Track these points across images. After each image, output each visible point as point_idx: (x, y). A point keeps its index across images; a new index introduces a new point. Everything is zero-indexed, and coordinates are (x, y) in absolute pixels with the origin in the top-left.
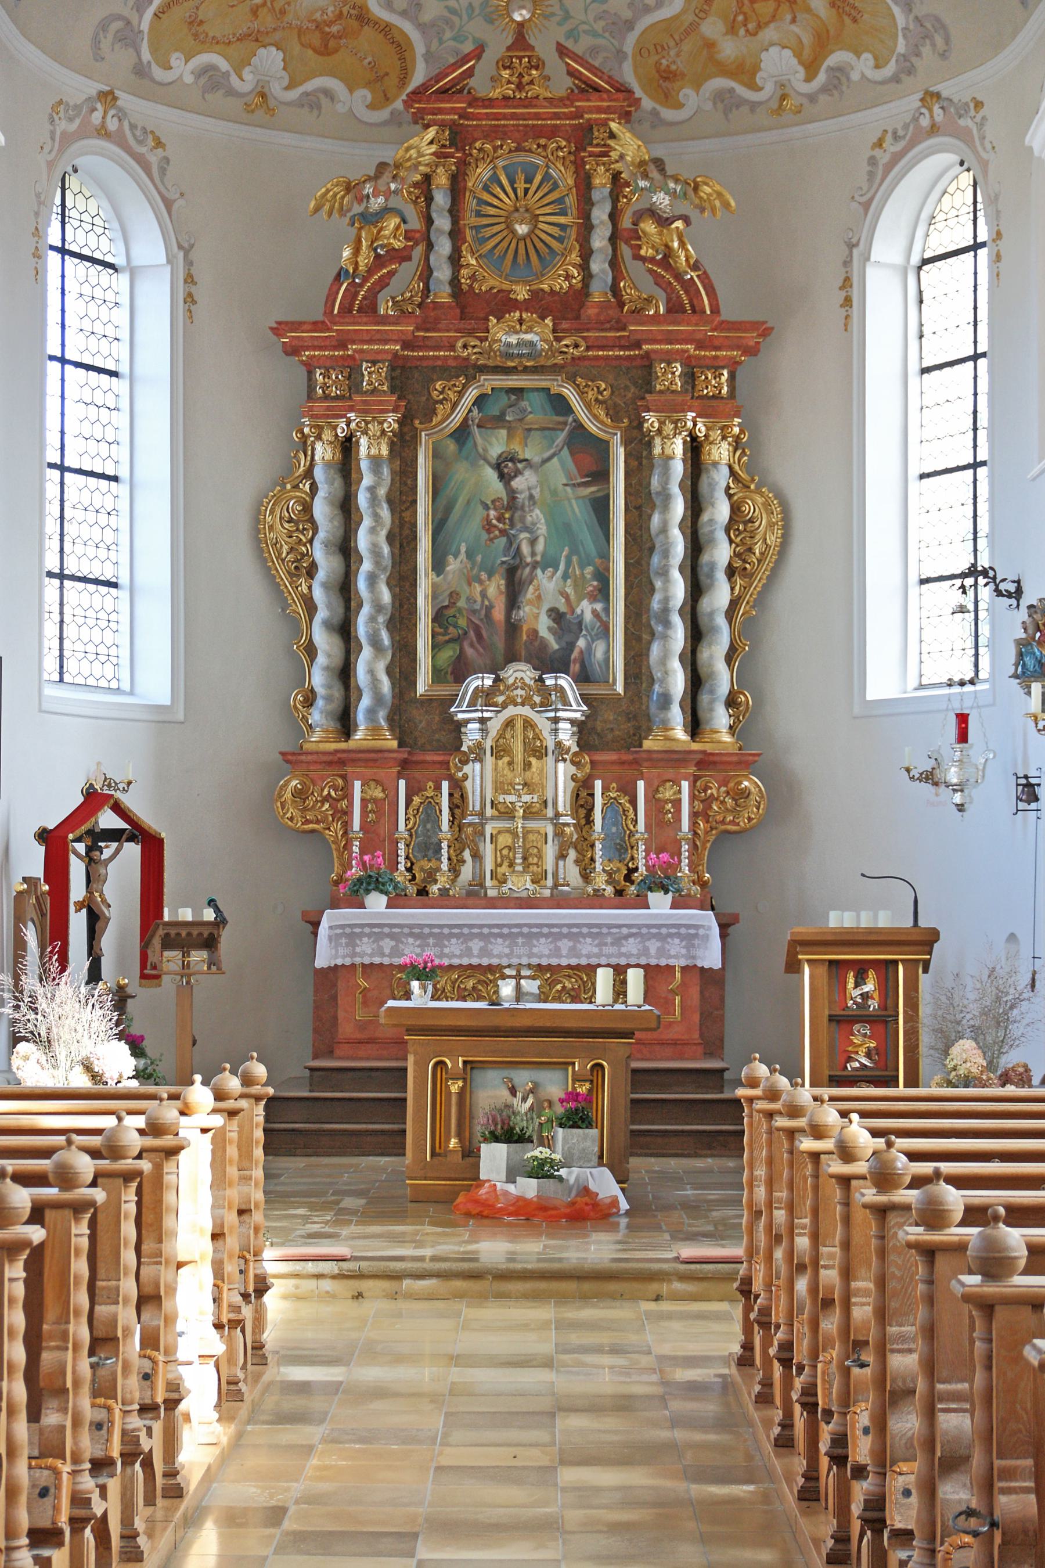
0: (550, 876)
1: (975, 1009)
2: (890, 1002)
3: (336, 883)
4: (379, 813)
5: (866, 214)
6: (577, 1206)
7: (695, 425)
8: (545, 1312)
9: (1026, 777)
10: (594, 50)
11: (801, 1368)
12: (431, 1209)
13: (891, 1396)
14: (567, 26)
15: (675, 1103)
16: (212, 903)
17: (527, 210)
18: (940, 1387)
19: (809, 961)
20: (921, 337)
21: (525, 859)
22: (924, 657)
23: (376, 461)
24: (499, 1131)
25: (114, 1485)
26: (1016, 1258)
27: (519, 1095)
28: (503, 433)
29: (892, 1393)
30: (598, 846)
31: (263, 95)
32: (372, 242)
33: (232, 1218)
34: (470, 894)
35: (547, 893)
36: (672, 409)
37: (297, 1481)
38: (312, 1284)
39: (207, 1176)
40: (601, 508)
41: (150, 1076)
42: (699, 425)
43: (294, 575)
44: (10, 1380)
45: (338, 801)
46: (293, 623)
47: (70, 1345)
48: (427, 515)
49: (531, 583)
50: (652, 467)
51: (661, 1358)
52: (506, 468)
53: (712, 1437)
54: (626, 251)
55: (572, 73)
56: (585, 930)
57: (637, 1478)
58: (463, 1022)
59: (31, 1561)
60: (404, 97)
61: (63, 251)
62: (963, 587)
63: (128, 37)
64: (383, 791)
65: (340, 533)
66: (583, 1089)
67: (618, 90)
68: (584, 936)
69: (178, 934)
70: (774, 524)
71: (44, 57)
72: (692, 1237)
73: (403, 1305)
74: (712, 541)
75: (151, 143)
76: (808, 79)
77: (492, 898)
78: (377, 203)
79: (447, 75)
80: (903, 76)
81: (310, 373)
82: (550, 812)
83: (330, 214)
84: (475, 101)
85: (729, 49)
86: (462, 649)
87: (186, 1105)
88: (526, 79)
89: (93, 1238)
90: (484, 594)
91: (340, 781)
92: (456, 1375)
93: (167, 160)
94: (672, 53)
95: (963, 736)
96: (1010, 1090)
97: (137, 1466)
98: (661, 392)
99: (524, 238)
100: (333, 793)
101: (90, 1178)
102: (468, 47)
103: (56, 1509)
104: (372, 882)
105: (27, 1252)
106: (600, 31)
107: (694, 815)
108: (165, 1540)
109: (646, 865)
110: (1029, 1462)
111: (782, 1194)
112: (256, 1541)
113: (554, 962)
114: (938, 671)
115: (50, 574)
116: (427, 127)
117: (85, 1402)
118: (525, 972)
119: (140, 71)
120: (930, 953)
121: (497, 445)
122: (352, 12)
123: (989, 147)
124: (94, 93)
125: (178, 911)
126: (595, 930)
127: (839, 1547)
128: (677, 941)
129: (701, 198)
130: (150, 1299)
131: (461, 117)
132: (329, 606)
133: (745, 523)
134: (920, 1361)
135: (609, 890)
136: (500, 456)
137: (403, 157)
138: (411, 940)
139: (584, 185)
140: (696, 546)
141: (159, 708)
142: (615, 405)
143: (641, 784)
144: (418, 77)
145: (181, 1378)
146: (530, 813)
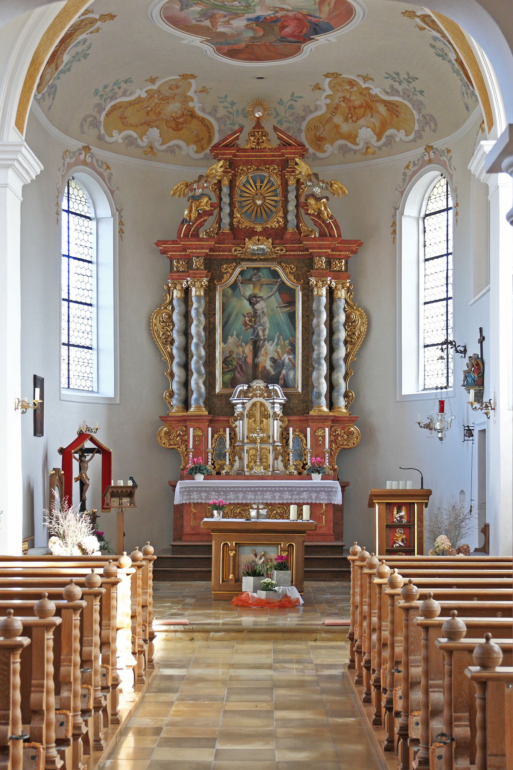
0: (271, 467)
1: (446, 522)
2: (411, 519)
3: (183, 470)
4: (200, 441)
5: (402, 196)
6: (282, 602)
7: (331, 283)
8: (269, 646)
9: (468, 427)
10: (289, 129)
11: (374, 671)
12: (222, 603)
13: (411, 684)
14: (279, 118)
15: (322, 560)
16: (131, 478)
17: (261, 194)
18: (431, 682)
19: (378, 503)
20: (425, 246)
21: (261, 460)
22: (426, 377)
23: (198, 297)
24: (250, 572)
25: (91, 720)
26: (462, 632)
27: (258, 557)
28: (252, 286)
29: (411, 683)
30: (291, 454)
31: (151, 147)
32: (197, 208)
33: (139, 609)
34: (238, 474)
35: (270, 473)
36: (321, 276)
37: (167, 716)
39: (129, 593)
40: (292, 316)
41: (106, 549)
42: (333, 283)
43: (165, 344)
44: (47, 680)
45: (183, 436)
46: (165, 363)
47: (72, 664)
48: (220, 319)
49: (263, 346)
50: (313, 299)
51: (317, 665)
52: (252, 300)
53: (337, 698)
54: (302, 211)
55: (279, 138)
56: (286, 489)
57: (307, 715)
58: (235, 527)
59: (56, 753)
60: (210, 148)
61: (68, 212)
62: (442, 349)
63: (95, 124)
64: (202, 432)
65: (184, 327)
66: (285, 554)
67: (299, 145)
68: (285, 491)
69: (117, 491)
70: (364, 323)
71: (60, 132)
72: (330, 615)
73: (211, 643)
74: (338, 330)
76: (379, 139)
77: (247, 476)
78: (199, 192)
79: (228, 139)
80: (417, 139)
81: (171, 262)
82: (271, 441)
83: (179, 196)
84: (239, 150)
85: (345, 128)
86: (234, 374)
87: (120, 564)
88: (261, 141)
89: (82, 621)
90: (243, 352)
91: (184, 428)
92: (233, 672)
93: (112, 174)
94: (321, 130)
95: (442, 410)
96: (461, 556)
97: (101, 712)
98: (317, 269)
99: (260, 206)
100: (181, 433)
101: (80, 596)
102: (236, 128)
103: (67, 731)
104: (197, 469)
105: (54, 628)
106: (292, 121)
107: (331, 442)
108: (112, 742)
109: (311, 462)
110: (467, 714)
111: (366, 600)
112: (149, 742)
113: (273, 502)
114: (432, 383)
115: (64, 344)
116: (219, 160)
117: (79, 688)
118: (261, 507)
119: (100, 138)
120: (428, 500)
121: (249, 290)
122: (188, 113)
123: (453, 168)
124: (81, 147)
125: (118, 482)
126: (290, 489)
127: (390, 744)
128: (323, 493)
129: (333, 189)
130: (106, 644)
131: (233, 156)
132: (179, 357)
133: (352, 323)
134: (423, 671)
135: (296, 472)
136: (250, 295)
137: (210, 173)
138: (214, 493)
139: (285, 184)
140: (331, 332)
141: (109, 398)
142: (298, 274)
143: (309, 429)
144: (216, 140)
145: (118, 676)
146: (263, 441)
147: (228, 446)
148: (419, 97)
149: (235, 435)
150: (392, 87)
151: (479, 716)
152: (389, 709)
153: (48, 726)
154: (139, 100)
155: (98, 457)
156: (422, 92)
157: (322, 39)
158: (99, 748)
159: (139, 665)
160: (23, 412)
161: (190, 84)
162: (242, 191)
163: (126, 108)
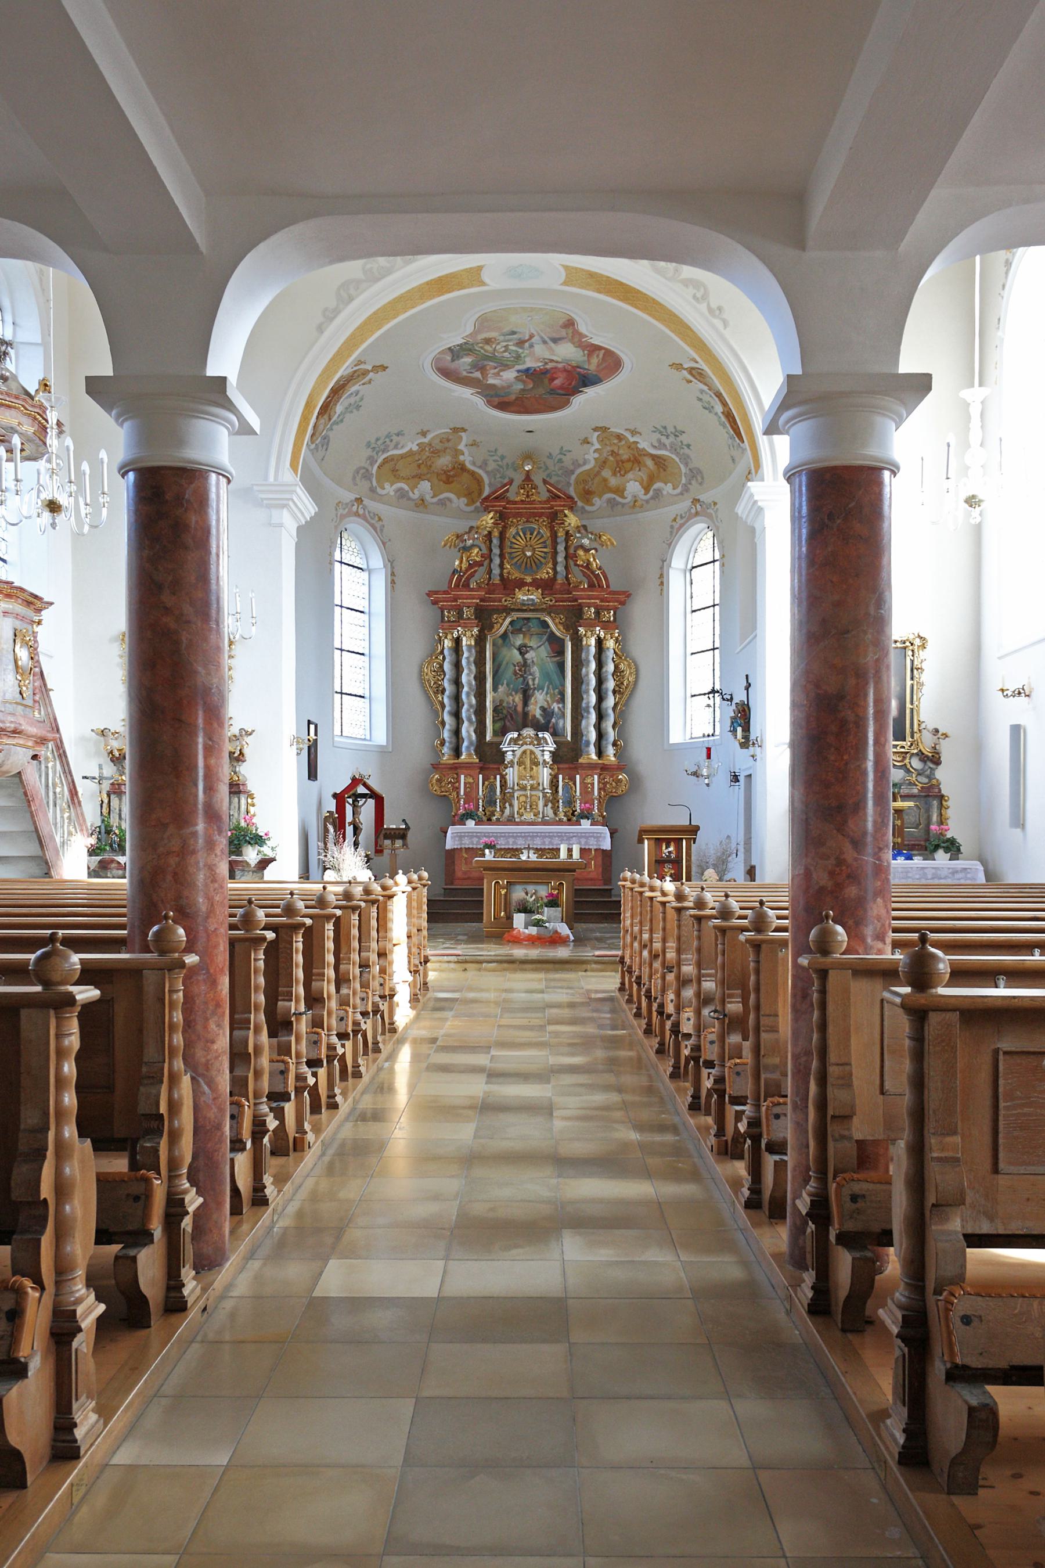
8: (541, 975)
10: (558, 482)
13: (683, 982)
14: (548, 472)
15: (593, 902)
34: (508, 820)
36: (590, 626)
38: (446, 965)
40: (561, 666)
43: (436, 693)
46: (436, 712)
52: (523, 650)
54: (571, 563)
55: (549, 491)
63: (367, 476)
74: (606, 680)
75: (377, 518)
81: (442, 612)
82: (541, 788)
84: (509, 502)
89: (360, 921)
90: (513, 701)
92: (504, 995)
95: (709, 757)
102: (506, 481)
103: (347, 1025)
104: (469, 815)
107: (600, 789)
112: (425, 1049)
117: (358, 986)
119: (372, 490)
121: (519, 640)
125: (391, 823)
130: (382, 954)
135: (565, 819)
139: (554, 536)
140: (600, 681)
143: (578, 777)
144: (486, 492)
146: (532, 788)
147: (498, 793)
148: (686, 451)
149: (506, 782)
150: (659, 441)
151: (752, 997)
152: (661, 1012)
153: (329, 1014)
154: (411, 453)
155: (371, 802)
156: (688, 446)
157: (591, 392)
158: (377, 1050)
159: (414, 981)
160: (298, 754)
161: (461, 437)
162: (512, 543)
163: (398, 460)
